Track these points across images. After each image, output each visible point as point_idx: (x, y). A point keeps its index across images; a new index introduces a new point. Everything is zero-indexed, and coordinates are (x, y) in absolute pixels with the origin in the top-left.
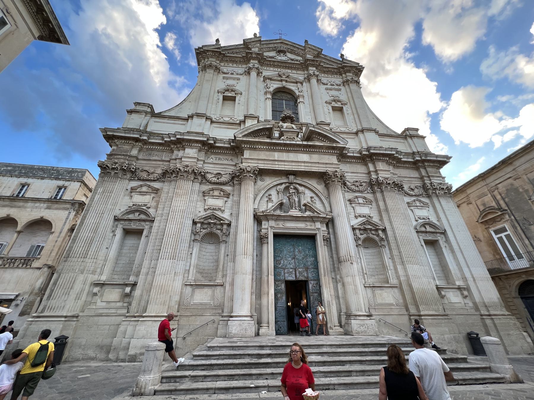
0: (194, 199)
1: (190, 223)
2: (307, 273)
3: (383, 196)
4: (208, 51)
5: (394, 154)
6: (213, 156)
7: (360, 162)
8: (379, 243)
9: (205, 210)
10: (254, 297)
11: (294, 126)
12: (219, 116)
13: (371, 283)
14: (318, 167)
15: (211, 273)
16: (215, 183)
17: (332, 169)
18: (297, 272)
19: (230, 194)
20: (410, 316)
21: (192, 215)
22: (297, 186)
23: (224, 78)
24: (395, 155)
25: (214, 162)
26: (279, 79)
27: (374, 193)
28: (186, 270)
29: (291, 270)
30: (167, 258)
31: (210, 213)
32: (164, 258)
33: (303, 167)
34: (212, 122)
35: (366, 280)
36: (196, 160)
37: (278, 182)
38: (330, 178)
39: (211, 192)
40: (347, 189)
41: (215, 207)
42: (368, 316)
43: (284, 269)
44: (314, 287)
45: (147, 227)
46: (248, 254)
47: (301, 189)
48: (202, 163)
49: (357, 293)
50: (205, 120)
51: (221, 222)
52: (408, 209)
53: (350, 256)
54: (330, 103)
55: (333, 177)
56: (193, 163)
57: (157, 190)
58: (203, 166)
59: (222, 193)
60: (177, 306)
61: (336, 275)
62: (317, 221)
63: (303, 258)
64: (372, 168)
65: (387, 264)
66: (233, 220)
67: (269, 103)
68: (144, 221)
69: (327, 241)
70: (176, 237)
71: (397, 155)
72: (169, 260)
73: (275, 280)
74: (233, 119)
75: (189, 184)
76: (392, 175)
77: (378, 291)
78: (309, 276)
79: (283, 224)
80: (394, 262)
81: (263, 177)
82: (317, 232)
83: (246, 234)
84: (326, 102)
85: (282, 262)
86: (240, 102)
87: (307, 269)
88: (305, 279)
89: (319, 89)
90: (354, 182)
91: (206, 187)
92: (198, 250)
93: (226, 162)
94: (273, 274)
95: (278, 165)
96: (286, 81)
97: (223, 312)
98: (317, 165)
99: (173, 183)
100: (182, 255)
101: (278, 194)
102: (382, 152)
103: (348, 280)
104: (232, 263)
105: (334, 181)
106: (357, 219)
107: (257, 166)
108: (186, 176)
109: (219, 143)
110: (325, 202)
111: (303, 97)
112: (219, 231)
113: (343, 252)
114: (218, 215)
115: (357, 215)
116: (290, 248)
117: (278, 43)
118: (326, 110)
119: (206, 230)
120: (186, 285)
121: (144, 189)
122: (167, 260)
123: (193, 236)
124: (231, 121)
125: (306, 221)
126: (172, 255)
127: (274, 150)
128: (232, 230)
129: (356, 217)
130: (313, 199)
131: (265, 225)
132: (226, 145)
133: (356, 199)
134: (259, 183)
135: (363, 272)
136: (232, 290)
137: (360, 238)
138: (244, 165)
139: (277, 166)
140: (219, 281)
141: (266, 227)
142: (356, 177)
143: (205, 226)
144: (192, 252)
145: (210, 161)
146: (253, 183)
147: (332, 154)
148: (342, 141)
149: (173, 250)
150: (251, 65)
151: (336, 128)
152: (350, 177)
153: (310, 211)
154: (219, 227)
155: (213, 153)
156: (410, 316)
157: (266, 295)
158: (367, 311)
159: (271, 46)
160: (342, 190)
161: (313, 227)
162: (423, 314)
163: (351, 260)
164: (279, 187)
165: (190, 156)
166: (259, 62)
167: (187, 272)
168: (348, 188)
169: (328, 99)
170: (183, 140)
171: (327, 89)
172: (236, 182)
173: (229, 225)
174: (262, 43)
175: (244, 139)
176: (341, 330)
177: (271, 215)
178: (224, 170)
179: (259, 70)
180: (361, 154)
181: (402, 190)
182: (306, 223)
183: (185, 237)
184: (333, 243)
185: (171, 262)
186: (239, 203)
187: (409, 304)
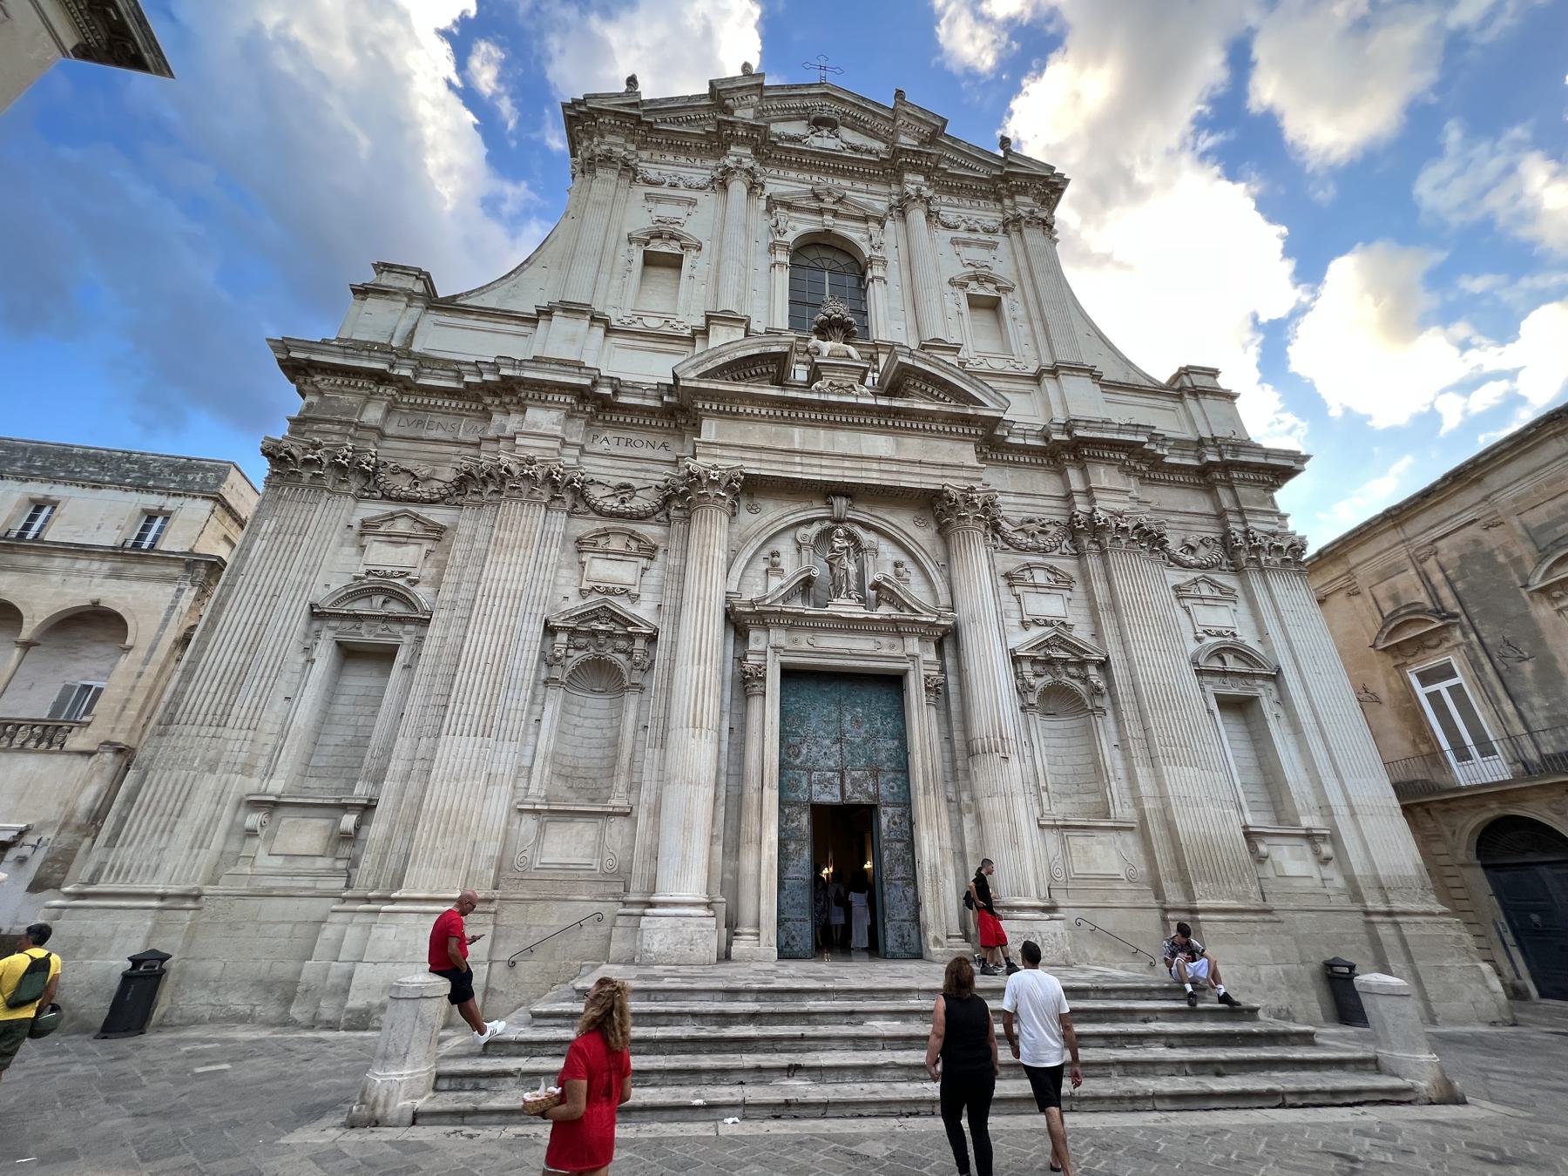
0: (551, 561)
2: (876, 784)
3: (1106, 564)
4: (601, 112)
5: (1144, 443)
6: (609, 434)
7: (1042, 465)
8: (1087, 702)
9: (582, 593)
11: (852, 350)
12: (629, 313)
15: (594, 779)
16: (612, 515)
18: (848, 781)
19: (656, 548)
20: (1166, 911)
21: (541, 607)
22: (858, 530)
25: (613, 451)
26: (814, 205)
29: (830, 774)
30: (465, 733)
32: (458, 733)
33: (875, 475)
34: (609, 331)
35: (1046, 807)
36: (557, 445)
37: (802, 516)
38: (953, 508)
39: (602, 541)
40: (1000, 543)
41: (611, 586)
42: (1044, 909)
43: (810, 771)
44: (895, 823)
45: (407, 639)
46: (704, 725)
47: (867, 538)
48: (576, 452)
49: (1015, 843)
50: (587, 323)
51: (630, 629)
52: (1177, 606)
56: (548, 453)
59: (633, 544)
60: (492, 872)
61: (958, 792)
62: (911, 634)
63: (866, 741)
64: (1076, 482)
66: (665, 626)
67: (782, 278)
68: (400, 620)
69: (938, 692)
70: (494, 671)
71: (1153, 447)
72: (479, 738)
74: (672, 322)
76: (1135, 505)
77: (1077, 841)
78: (881, 792)
79: (811, 641)
82: (910, 665)
83: (702, 668)
84: (952, 282)
85: (804, 752)
86: (694, 272)
87: (876, 772)
88: (870, 801)
89: (932, 240)
90: (1022, 522)
91: (586, 526)
93: (647, 452)
94: (776, 783)
95: (801, 464)
96: (835, 214)
97: (627, 890)
98: (917, 470)
99: (488, 511)
100: (511, 723)
101: (799, 550)
103: (991, 806)
105: (964, 517)
108: (526, 491)
109: (627, 395)
110: (936, 577)
111: (885, 263)
112: (621, 657)
113: (981, 726)
114: (620, 608)
116: (830, 712)
120: (521, 811)
121: (402, 526)
123: (544, 668)
124: (667, 330)
125: (878, 633)
126: (481, 724)
127: (793, 422)
128: (660, 654)
129: (1025, 625)
130: (901, 570)
131: (757, 641)
134: (745, 517)
135: (1037, 785)
137: (1032, 687)
138: (700, 464)
139: (799, 469)
140: (618, 802)
141: (760, 647)
143: (582, 641)
146: (725, 519)
147: (963, 438)
148: (993, 400)
150: (730, 161)
151: (981, 360)
153: (890, 603)
156: (1166, 911)
157: (754, 847)
158: (1043, 895)
161: (897, 652)
162: (1203, 906)
164: (802, 530)
165: (541, 431)
166: (756, 152)
167: (524, 773)
169: (959, 271)
170: (522, 382)
173: (652, 639)
177: (776, 612)
178: (642, 475)
179: (754, 177)
180: (1046, 439)
182: (878, 639)
184: (953, 698)
185: (478, 745)
186: (681, 575)
187: (1163, 878)
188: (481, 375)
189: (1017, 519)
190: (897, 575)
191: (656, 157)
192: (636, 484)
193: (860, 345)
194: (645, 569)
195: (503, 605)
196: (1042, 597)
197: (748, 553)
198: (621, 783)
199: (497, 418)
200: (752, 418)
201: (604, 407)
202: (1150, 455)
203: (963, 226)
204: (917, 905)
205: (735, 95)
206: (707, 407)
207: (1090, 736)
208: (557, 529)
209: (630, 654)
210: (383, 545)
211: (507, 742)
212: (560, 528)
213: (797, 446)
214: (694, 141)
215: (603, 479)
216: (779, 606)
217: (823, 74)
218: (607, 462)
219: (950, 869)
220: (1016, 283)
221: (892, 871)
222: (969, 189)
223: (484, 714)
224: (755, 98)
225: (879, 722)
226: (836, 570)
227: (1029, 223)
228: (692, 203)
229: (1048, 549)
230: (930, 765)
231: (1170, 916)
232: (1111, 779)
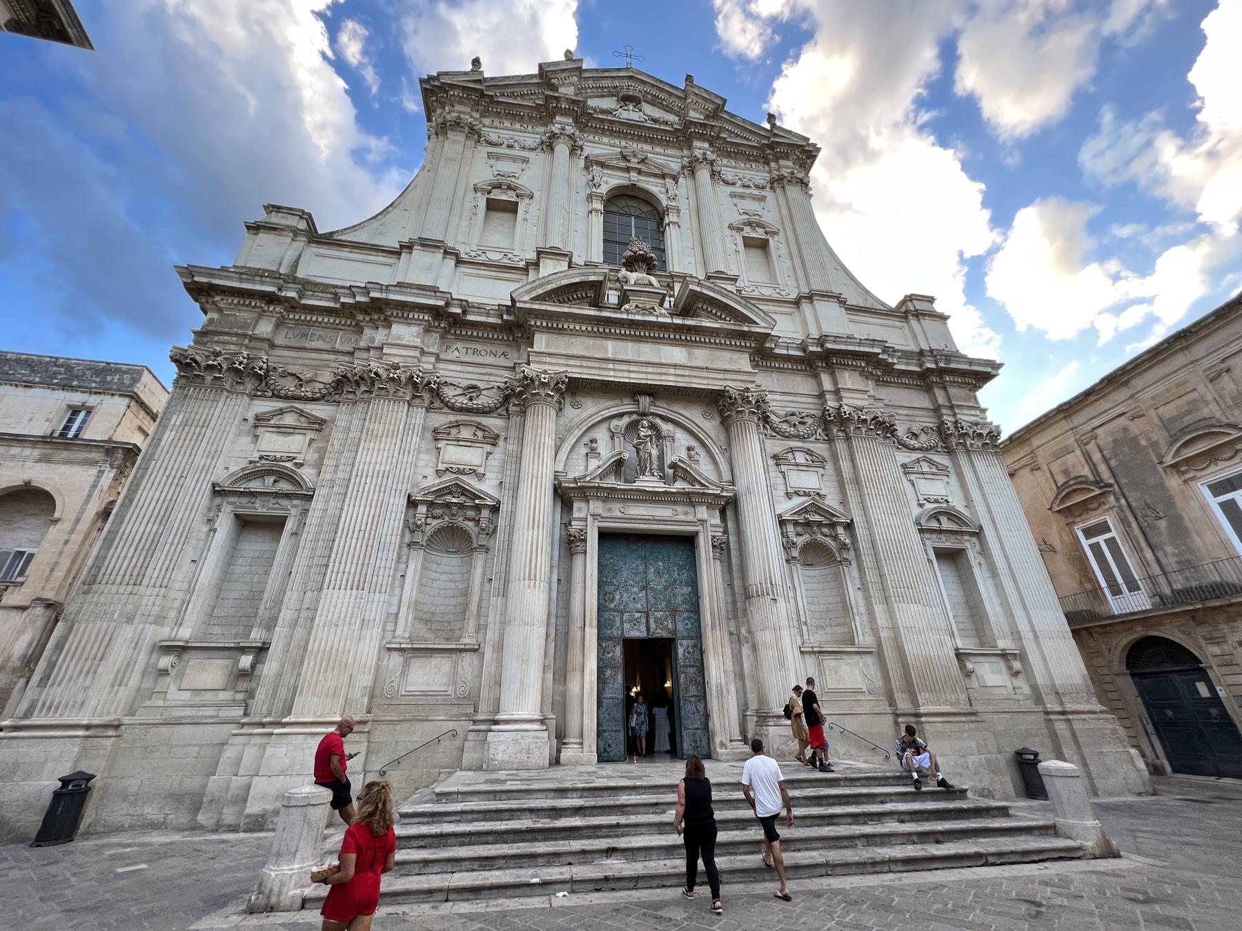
0: (412, 447)
1: (401, 502)
2: (674, 622)
4: (452, 86)
6: (459, 345)
7: (801, 370)
8: (837, 555)
11: (653, 280)
12: (475, 248)
16: (462, 410)
18: (652, 620)
22: (658, 421)
23: (490, 155)
24: (880, 356)
25: (463, 359)
26: (623, 164)
27: (830, 440)
28: (389, 614)
29: (638, 615)
30: (343, 587)
31: (450, 480)
32: (337, 588)
33: (672, 378)
34: (459, 262)
35: (806, 637)
36: (417, 353)
37: (614, 411)
38: (733, 404)
39: (454, 431)
40: (770, 432)
41: (462, 467)
44: (689, 653)
45: (294, 511)
47: (666, 428)
48: (433, 360)
51: (477, 502)
52: (904, 479)
53: (772, 584)
54: (740, 230)
55: (740, 401)
56: (409, 360)
57: (322, 422)
59: (480, 434)
62: (700, 503)
63: (666, 588)
64: (827, 385)
67: (598, 222)
68: (288, 496)
69: (722, 549)
71: (885, 357)
72: (354, 591)
73: (601, 638)
74: (510, 256)
76: (872, 401)
77: (829, 662)
78: (678, 628)
80: (867, 598)
82: (700, 528)
84: (731, 227)
85: (617, 597)
86: (527, 216)
87: (674, 612)
88: (670, 636)
89: (715, 193)
92: (419, 566)
93: (489, 360)
94: (595, 623)
95: (614, 370)
96: (640, 172)
97: (476, 711)
98: (705, 374)
99: (361, 406)
100: (380, 578)
101: (612, 438)
103: (765, 637)
108: (392, 391)
109: (474, 313)
110: (720, 459)
111: (678, 211)
112: (471, 524)
113: (756, 576)
114: (469, 484)
115: (790, 490)
116: (637, 565)
117: (623, 77)
119: (440, 521)
120: (390, 649)
121: (289, 419)
124: (506, 262)
125: (675, 503)
126: (356, 579)
127: (607, 336)
128: (502, 522)
129: (788, 495)
130: (692, 453)
131: (579, 510)
133: (790, 455)
134: (569, 411)
136: (499, 661)
137: (794, 544)
138: (533, 369)
139: (612, 373)
140: (468, 640)
141: (582, 515)
142: (792, 405)
143: (438, 511)
146: (553, 413)
147: (740, 349)
151: (752, 288)
153: (684, 479)
156: (897, 715)
157: (578, 674)
161: (690, 518)
163: (773, 591)
164: (615, 422)
165: (404, 342)
166: (576, 121)
168: (773, 429)
169: (736, 218)
170: (387, 302)
171: (733, 195)
172: (515, 408)
173: (495, 509)
175: (536, 307)
178: (486, 378)
179: (575, 141)
180: (804, 350)
182: (674, 507)
184: (734, 553)
185: (353, 597)
186: (519, 458)
188: (354, 297)
189: (783, 413)
190: (690, 457)
192: (481, 385)
195: (374, 483)
197: (572, 440)
198: (471, 625)
199: (368, 332)
200: (574, 333)
201: (455, 323)
203: (739, 183)
204: (707, 716)
206: (538, 324)
207: (839, 581)
208: (418, 422)
209: (477, 522)
210: (274, 435)
218: (458, 368)
219: (732, 688)
221: (687, 690)
223: (358, 571)
224: (575, 79)
225: (676, 573)
228: (525, 161)
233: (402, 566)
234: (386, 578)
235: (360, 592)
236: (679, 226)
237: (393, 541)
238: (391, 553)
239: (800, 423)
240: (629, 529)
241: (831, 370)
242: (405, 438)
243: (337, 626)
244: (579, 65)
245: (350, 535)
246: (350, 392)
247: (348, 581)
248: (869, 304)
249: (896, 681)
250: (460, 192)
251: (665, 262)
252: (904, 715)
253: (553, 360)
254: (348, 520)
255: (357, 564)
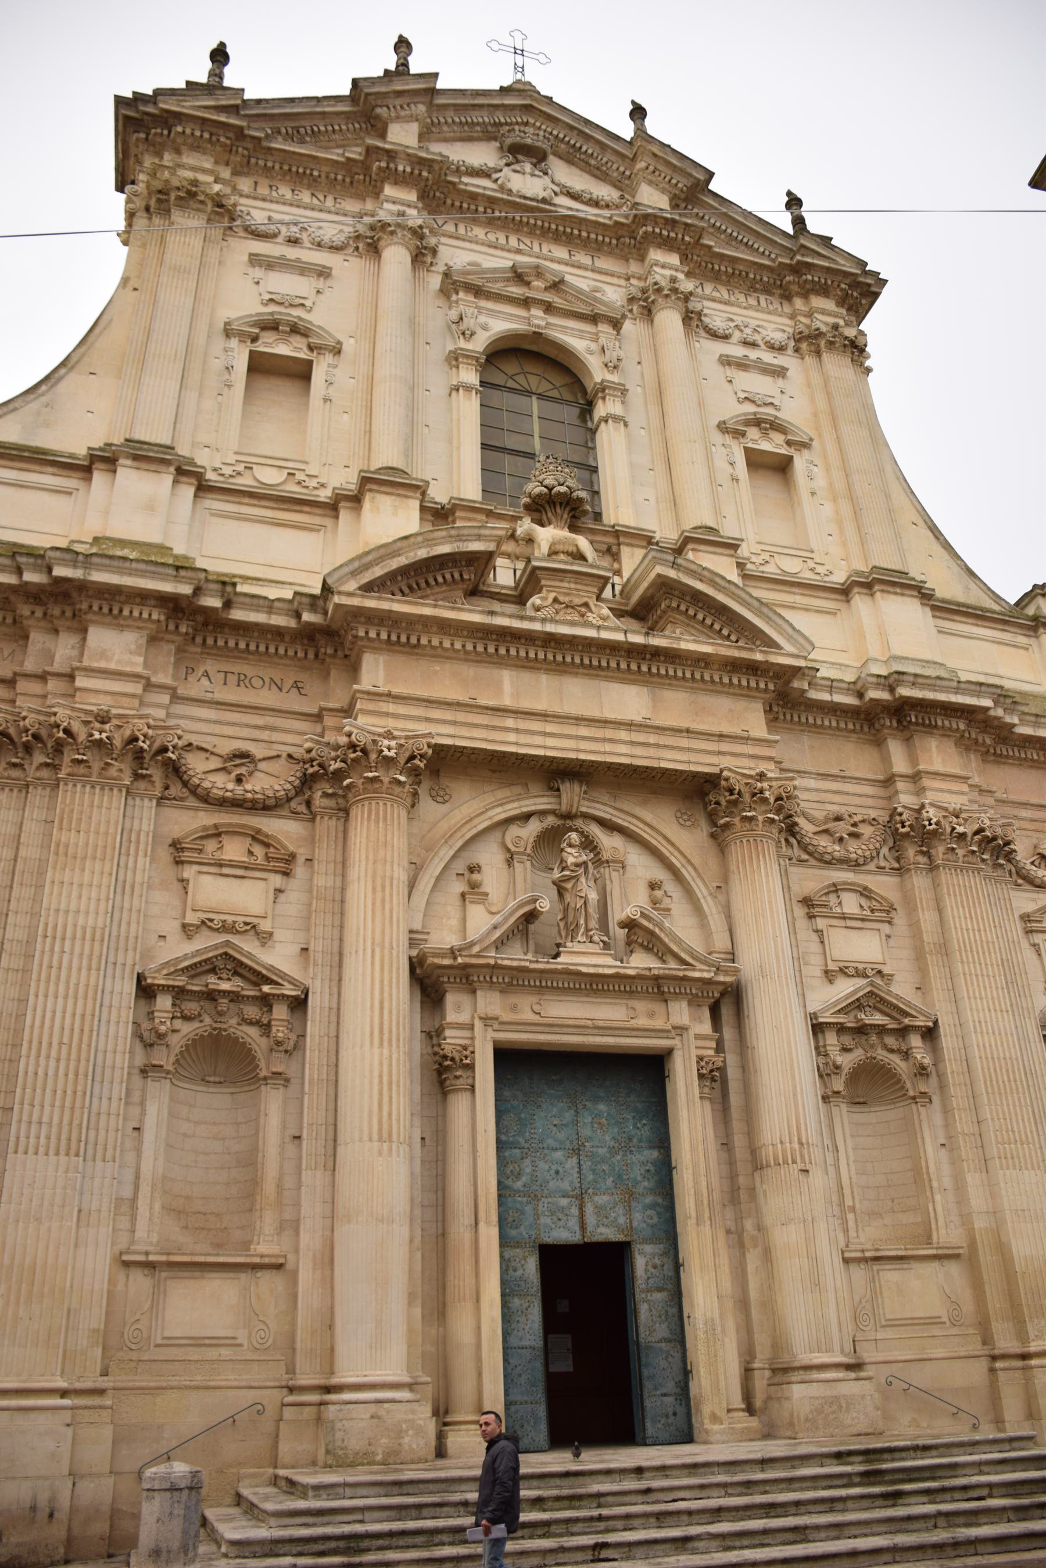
0: (138, 879)
3: (936, 885)
4: (179, 117)
5: (988, 709)
6: (210, 665)
7: (853, 731)
8: (908, 1085)
10: (418, 1311)
11: (583, 543)
12: (232, 458)
13: (869, 1246)
14: (689, 750)
15: (218, 1215)
17: (746, 762)
18: (589, 1209)
19: (293, 856)
20: (994, 1358)
21: (130, 953)
23: (255, 260)
24: (992, 713)
25: (218, 696)
26: (516, 291)
28: (119, 1201)
29: (564, 1202)
30: (42, 1150)
31: (216, 947)
32: (31, 1150)
34: (203, 488)
35: (852, 1233)
36: (137, 688)
37: (514, 809)
38: (735, 803)
39: (211, 845)
40: (797, 852)
41: (230, 919)
42: (849, 1367)
44: (655, 1267)
46: (395, 1137)
47: (609, 842)
48: (165, 699)
50: (170, 478)
51: (266, 989)
52: (1025, 944)
55: (747, 798)
56: (125, 702)
58: (168, 715)
59: (259, 851)
60: (99, 1351)
61: (739, 1219)
62: (677, 996)
64: (900, 764)
65: (932, 1169)
66: (318, 983)
67: (470, 408)
69: (713, 1080)
70: (74, 1056)
71: (1000, 712)
72: (52, 1158)
73: (505, 1242)
74: (300, 476)
75: (115, 804)
76: (975, 795)
77: (890, 1276)
78: (635, 1224)
79: (536, 1008)
80: (955, 1162)
81: (445, 782)
82: (675, 1042)
83: (386, 1052)
84: (723, 427)
85: (528, 1170)
86: (331, 391)
87: (630, 1196)
88: (620, 1238)
89: (693, 356)
90: (826, 820)
92: (165, 1112)
93: (267, 697)
94: (494, 1218)
95: (516, 730)
96: (549, 308)
97: (291, 1370)
98: (684, 742)
99: (38, 796)
100: (102, 1133)
101: (510, 862)
102: (942, 697)
104: (319, 1174)
105: (751, 819)
106: (831, 982)
107: (424, 736)
108: (96, 766)
109: (245, 607)
110: (710, 906)
111: (624, 392)
112: (253, 1032)
114: (249, 956)
115: (832, 966)
117: (513, 107)
118: (721, 464)
119: (196, 1024)
120: (127, 1264)
122: (41, 1157)
123: (139, 1048)
124: (292, 489)
125: (631, 994)
126: (64, 1137)
127: (500, 661)
128: (315, 1026)
129: (829, 976)
130: (658, 893)
132: (279, 620)
133: (832, 898)
134: (428, 807)
139: (512, 737)
140: (265, 1248)
141: (464, 1017)
142: (838, 798)
143: (191, 1007)
144: (141, 1121)
145: (197, 687)
146: (404, 813)
147: (746, 693)
148: (789, 639)
149: (67, 1112)
150: (386, 212)
151: (766, 556)
152: (813, 796)
153: (648, 949)
154: (252, 1011)
155: (211, 651)
156: (994, 1358)
157: (469, 1305)
158: (847, 1350)
159: (477, 117)
160: (779, 856)
161: (658, 1023)
162: (1039, 1349)
163: (802, 1156)
164: (514, 831)
165: (112, 666)
166: (423, 196)
167: (125, 1208)
168: (804, 847)
169: (733, 410)
170: (82, 586)
171: (726, 361)
172: (326, 802)
173: (299, 1004)
174: (440, 101)
175: (371, 603)
176: (754, 1422)
177: (487, 966)
178: (265, 735)
179: (422, 237)
180: (860, 695)
181: (1009, 861)
183: (109, 1055)
184: (734, 1087)
185: (61, 1169)
187: (993, 1318)
188: (19, 572)
190: (655, 902)
191: (263, 191)
192: (258, 751)
193: (592, 531)
194: (279, 891)
195: (77, 950)
196: (852, 933)
197: (435, 868)
198: (268, 1221)
199: (38, 639)
200: (439, 654)
201: (206, 624)
202: (996, 723)
203: (737, 336)
204: (686, 1373)
205: (391, 102)
206: (372, 634)
207: (910, 1130)
208: (145, 827)
209: (266, 1028)
211: (99, 1163)
212: (148, 825)
213: (507, 701)
214: (325, 169)
215: (206, 742)
216: (492, 957)
217: (519, 60)
219: (731, 1325)
220: (812, 434)
221: (652, 1331)
222: (743, 276)
224: (422, 108)
226: (568, 897)
227: (832, 343)
228: (323, 273)
229: (861, 861)
230: (704, 1184)
231: (999, 1365)
232: (936, 1191)
233: (135, 1111)
234: (112, 1134)
235: (74, 1159)
236: (626, 425)
237: (118, 1064)
238: (116, 1086)
239: (850, 835)
240: (549, 1044)
241: (907, 734)
242: (123, 859)
243: (38, 1220)
244: (431, 85)
245: (43, 1052)
246: (15, 765)
247: (48, 1138)
248: (975, 598)
249: (995, 1301)
250: (200, 339)
251: (597, 493)
252: (1004, 1357)
253: (401, 709)
254: (37, 1023)
255: (63, 1107)
